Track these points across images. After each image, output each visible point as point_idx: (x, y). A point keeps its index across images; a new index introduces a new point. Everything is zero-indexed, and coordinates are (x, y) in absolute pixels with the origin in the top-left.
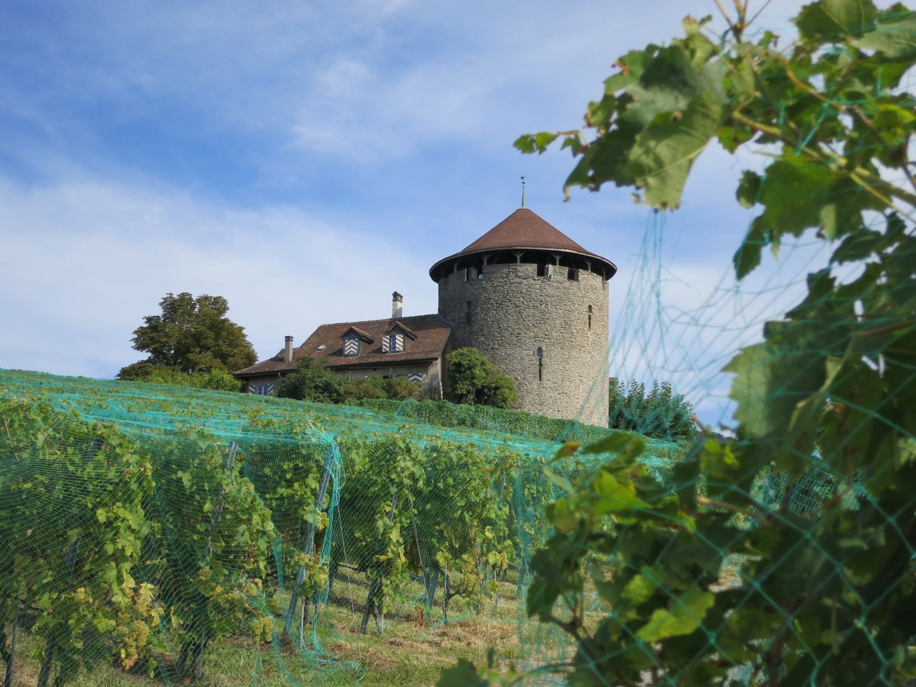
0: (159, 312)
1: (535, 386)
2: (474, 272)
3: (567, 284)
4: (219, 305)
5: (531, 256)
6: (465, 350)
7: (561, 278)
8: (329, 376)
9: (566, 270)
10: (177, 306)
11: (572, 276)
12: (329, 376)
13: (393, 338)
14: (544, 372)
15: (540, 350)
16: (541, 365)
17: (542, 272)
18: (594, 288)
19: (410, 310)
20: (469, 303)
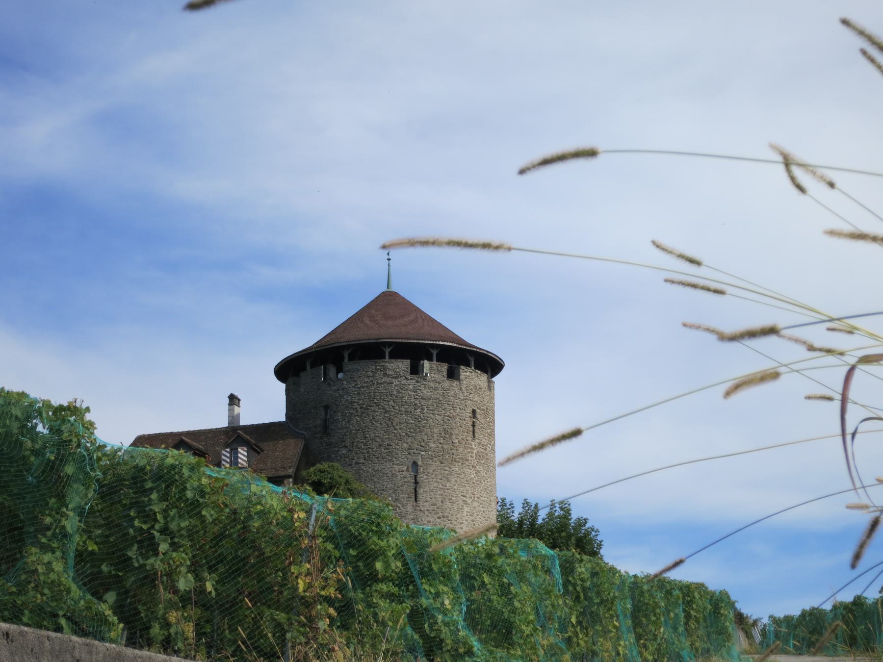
1: (409, 508)
2: (332, 370)
3: (447, 383)
6: (324, 466)
7: (438, 377)
9: (445, 367)
11: (452, 375)
13: (234, 452)
14: (420, 491)
15: (415, 464)
16: (416, 483)
17: (415, 370)
18: (478, 389)
19: (249, 417)
20: (327, 407)
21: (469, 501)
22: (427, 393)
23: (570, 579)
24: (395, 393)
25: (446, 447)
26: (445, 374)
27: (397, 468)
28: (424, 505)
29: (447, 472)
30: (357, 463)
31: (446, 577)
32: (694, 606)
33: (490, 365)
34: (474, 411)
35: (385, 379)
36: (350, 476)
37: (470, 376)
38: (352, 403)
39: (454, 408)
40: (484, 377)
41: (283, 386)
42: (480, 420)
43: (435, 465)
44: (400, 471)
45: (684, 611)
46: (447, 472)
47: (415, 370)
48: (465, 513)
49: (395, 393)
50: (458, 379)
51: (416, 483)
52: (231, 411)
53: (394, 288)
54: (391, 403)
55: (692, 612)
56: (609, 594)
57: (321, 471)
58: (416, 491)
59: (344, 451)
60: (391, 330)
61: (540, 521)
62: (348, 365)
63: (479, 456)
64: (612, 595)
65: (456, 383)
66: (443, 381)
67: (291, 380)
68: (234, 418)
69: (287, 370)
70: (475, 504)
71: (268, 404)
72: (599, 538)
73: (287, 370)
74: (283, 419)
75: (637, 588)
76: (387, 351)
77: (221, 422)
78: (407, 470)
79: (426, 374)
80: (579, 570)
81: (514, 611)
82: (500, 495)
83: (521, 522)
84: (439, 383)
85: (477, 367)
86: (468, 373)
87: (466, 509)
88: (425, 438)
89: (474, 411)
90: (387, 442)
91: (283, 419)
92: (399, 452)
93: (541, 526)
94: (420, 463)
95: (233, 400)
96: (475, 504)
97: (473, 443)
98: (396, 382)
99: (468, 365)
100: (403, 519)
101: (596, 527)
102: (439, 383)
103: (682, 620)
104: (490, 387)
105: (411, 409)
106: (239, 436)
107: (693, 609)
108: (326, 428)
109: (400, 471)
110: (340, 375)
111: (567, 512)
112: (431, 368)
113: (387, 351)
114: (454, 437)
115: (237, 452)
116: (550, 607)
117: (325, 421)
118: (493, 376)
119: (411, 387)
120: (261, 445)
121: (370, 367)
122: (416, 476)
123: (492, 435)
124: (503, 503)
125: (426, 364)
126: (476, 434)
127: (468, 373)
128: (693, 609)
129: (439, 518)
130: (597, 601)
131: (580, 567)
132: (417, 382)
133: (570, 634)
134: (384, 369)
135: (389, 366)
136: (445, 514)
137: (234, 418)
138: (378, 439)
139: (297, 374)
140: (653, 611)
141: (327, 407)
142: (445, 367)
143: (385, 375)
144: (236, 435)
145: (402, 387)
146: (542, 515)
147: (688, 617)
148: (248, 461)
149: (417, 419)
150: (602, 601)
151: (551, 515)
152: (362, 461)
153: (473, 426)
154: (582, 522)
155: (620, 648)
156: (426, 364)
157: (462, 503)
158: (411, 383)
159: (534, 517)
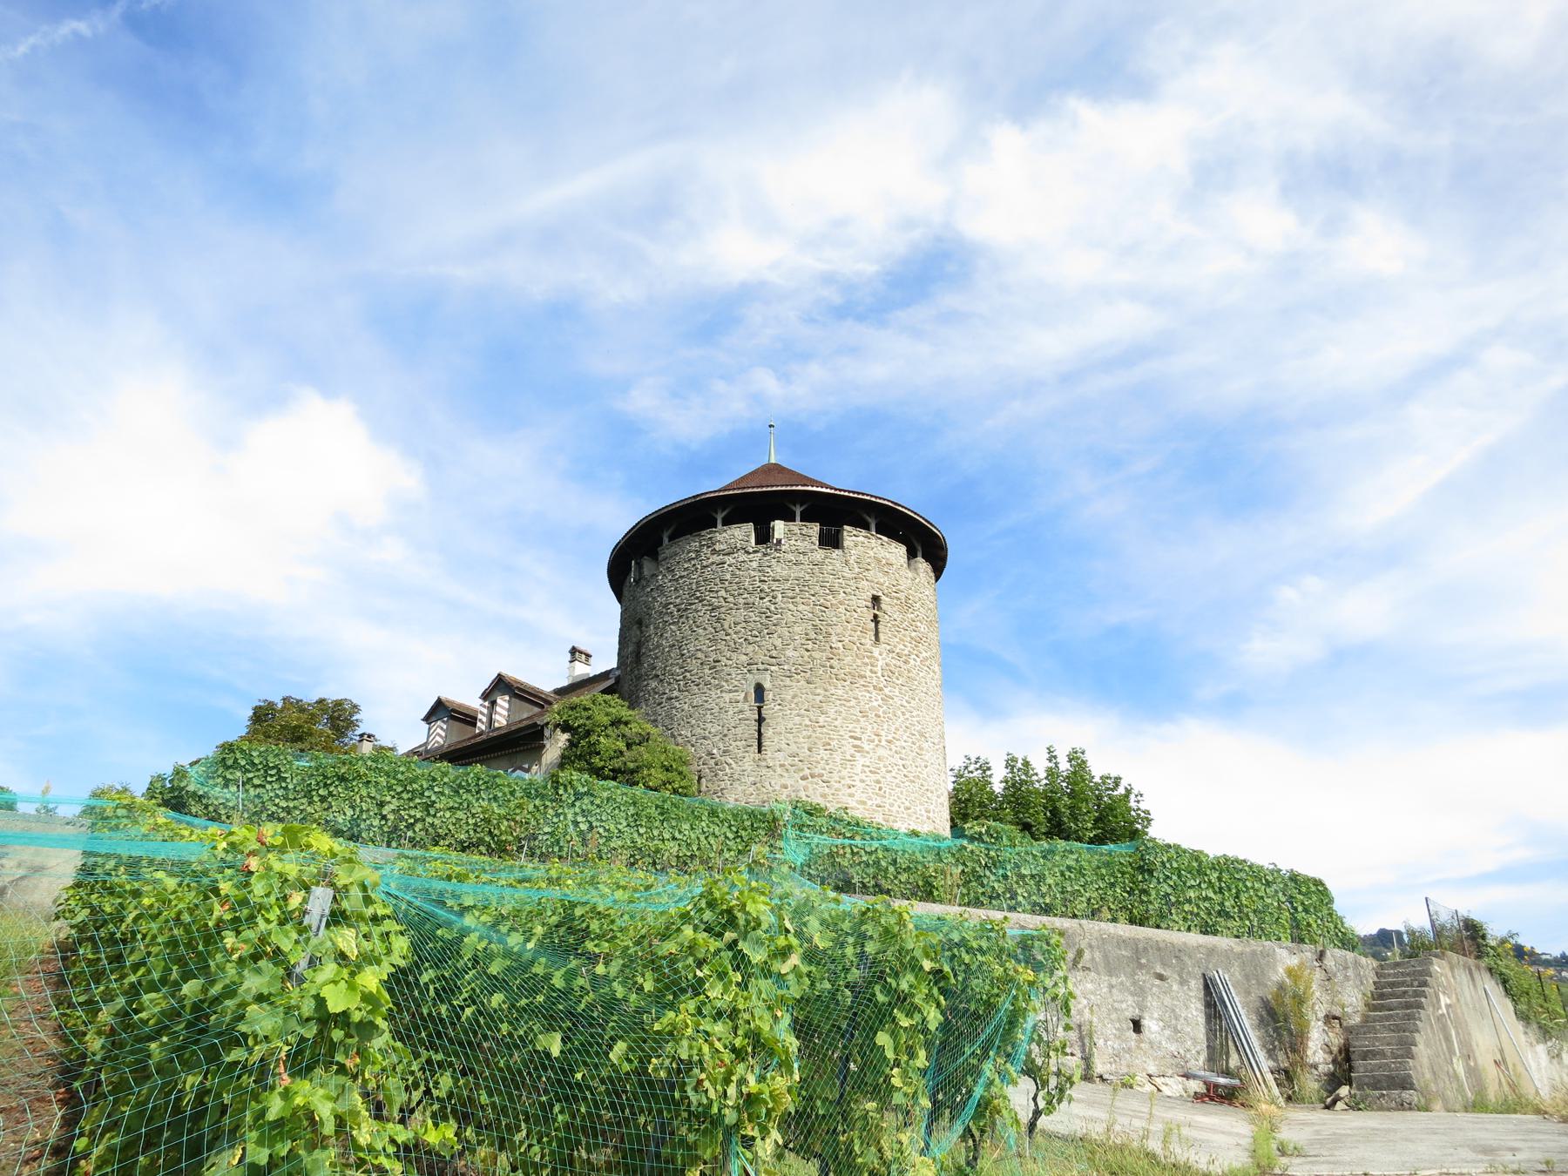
1: (748, 765)
3: (820, 554)
9: (814, 529)
11: (831, 540)
14: (768, 733)
15: (759, 690)
16: (761, 720)
17: (764, 537)
21: (866, 747)
22: (779, 570)
24: (728, 576)
25: (816, 655)
26: (816, 540)
27: (727, 697)
29: (819, 698)
35: (715, 558)
38: (666, 606)
46: (819, 698)
47: (764, 537)
48: (858, 769)
49: (728, 576)
54: (723, 593)
58: (760, 734)
59: (654, 684)
63: (890, 672)
66: (812, 551)
70: (881, 752)
78: (746, 699)
79: (779, 541)
82: (139, 788)
84: (804, 554)
85: (881, 530)
86: (861, 539)
87: (861, 760)
88: (778, 642)
90: (713, 656)
92: (733, 671)
94: (767, 685)
96: (881, 752)
97: (876, 652)
98: (729, 560)
100: (736, 784)
102: (804, 554)
114: (834, 638)
119: (755, 565)
122: (760, 708)
126: (881, 636)
127: (861, 539)
129: (803, 778)
132: (765, 555)
135: (718, 537)
136: (816, 771)
138: (699, 655)
142: (814, 529)
143: (714, 552)
146: (1040, 766)
152: (676, 693)
153: (875, 619)
157: (852, 751)
159: (985, 783)
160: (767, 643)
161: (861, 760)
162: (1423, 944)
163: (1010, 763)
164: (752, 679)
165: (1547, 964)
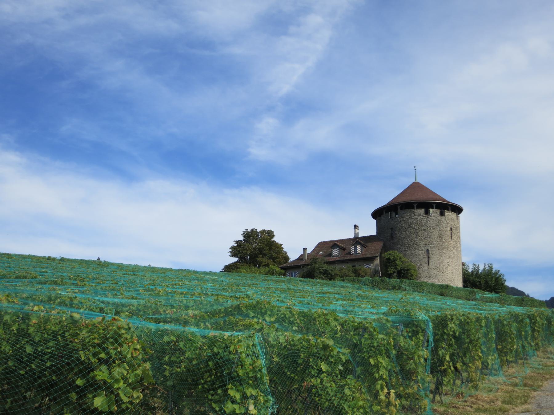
0: (241, 238)
1: (426, 268)
2: (394, 214)
3: (440, 218)
4: (270, 234)
5: (421, 205)
6: (391, 252)
7: (436, 215)
8: (326, 267)
9: (439, 211)
10: (250, 235)
11: (442, 214)
12: (326, 267)
13: (356, 247)
14: (430, 261)
15: (428, 250)
16: (429, 258)
17: (427, 213)
18: (453, 219)
19: (362, 233)
20: (392, 229)
22: (431, 222)
23: (445, 331)
28: (432, 266)
30: (405, 251)
31: (256, 382)
32: (537, 325)
33: (458, 210)
34: (451, 228)
35: (415, 217)
36: (401, 256)
37: (449, 214)
39: (443, 227)
40: (455, 215)
41: (375, 221)
42: (454, 232)
43: (436, 250)
44: (422, 253)
45: (531, 327)
50: (444, 216)
51: (429, 258)
52: (355, 231)
53: (417, 181)
55: (536, 328)
56: (475, 336)
57: (390, 254)
60: (417, 197)
61: (480, 272)
62: (400, 212)
63: (454, 246)
64: (477, 336)
65: (443, 217)
67: (378, 218)
68: (356, 234)
69: (376, 214)
71: (369, 228)
72: (504, 278)
73: (376, 214)
74: (375, 234)
75: (501, 323)
76: (415, 206)
77: (351, 235)
80: (450, 325)
81: (343, 397)
83: (472, 272)
85: (452, 211)
87: (449, 268)
89: (451, 228)
91: (375, 234)
93: (481, 273)
95: (356, 227)
99: (448, 210)
101: (503, 273)
103: (530, 333)
104: (458, 218)
105: (425, 228)
106: (357, 241)
107: (536, 326)
108: (392, 237)
109: (422, 253)
110: (397, 216)
111: (491, 268)
112: (433, 212)
113: (415, 206)
115: (357, 248)
116: (413, 364)
117: (392, 234)
118: (459, 214)
120: (366, 244)
121: (408, 212)
123: (459, 238)
124: (463, 264)
125: (431, 210)
128: (536, 326)
130: (468, 340)
131: (451, 323)
133: (446, 366)
134: (414, 213)
135: (416, 211)
137: (356, 234)
139: (380, 216)
140: (510, 336)
141: (392, 229)
142: (439, 211)
143: (415, 215)
144: (357, 241)
145: (422, 220)
147: (533, 331)
148: (361, 251)
149: (428, 232)
150: (471, 342)
151: (484, 269)
154: (497, 272)
155: (489, 361)
156: (431, 210)
158: (425, 218)
159: (478, 270)
160: (429, 239)
161: (449, 268)
162: (252, 387)
163: (474, 265)
164: (426, 248)
165: (540, 304)
